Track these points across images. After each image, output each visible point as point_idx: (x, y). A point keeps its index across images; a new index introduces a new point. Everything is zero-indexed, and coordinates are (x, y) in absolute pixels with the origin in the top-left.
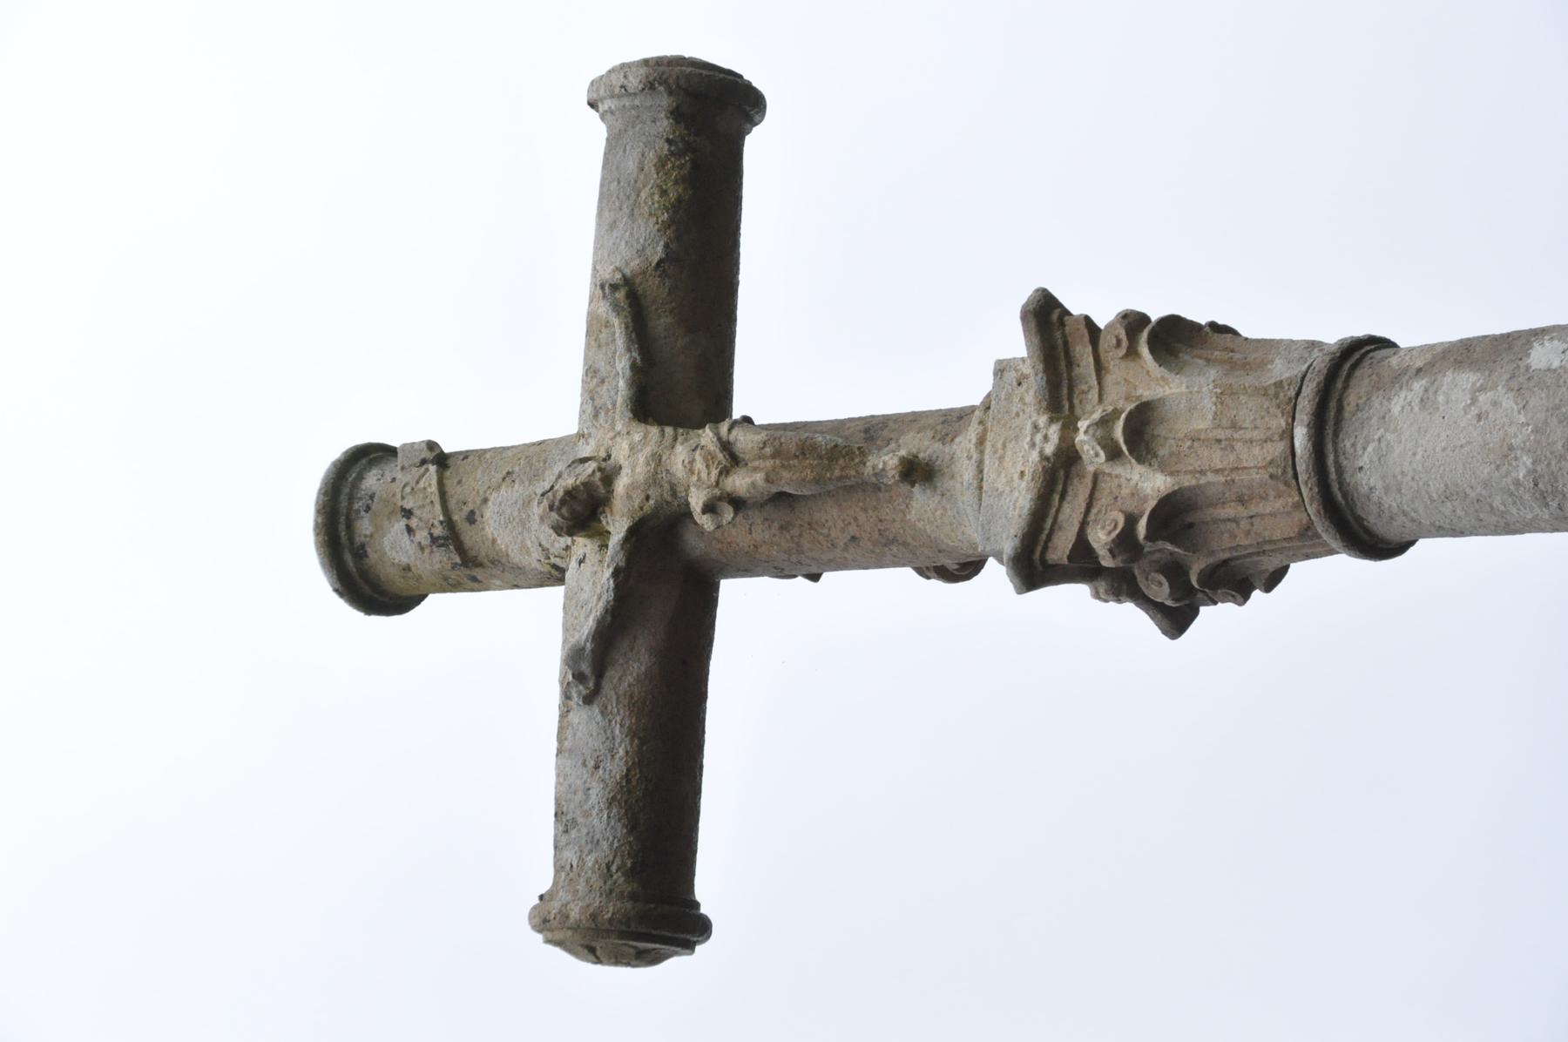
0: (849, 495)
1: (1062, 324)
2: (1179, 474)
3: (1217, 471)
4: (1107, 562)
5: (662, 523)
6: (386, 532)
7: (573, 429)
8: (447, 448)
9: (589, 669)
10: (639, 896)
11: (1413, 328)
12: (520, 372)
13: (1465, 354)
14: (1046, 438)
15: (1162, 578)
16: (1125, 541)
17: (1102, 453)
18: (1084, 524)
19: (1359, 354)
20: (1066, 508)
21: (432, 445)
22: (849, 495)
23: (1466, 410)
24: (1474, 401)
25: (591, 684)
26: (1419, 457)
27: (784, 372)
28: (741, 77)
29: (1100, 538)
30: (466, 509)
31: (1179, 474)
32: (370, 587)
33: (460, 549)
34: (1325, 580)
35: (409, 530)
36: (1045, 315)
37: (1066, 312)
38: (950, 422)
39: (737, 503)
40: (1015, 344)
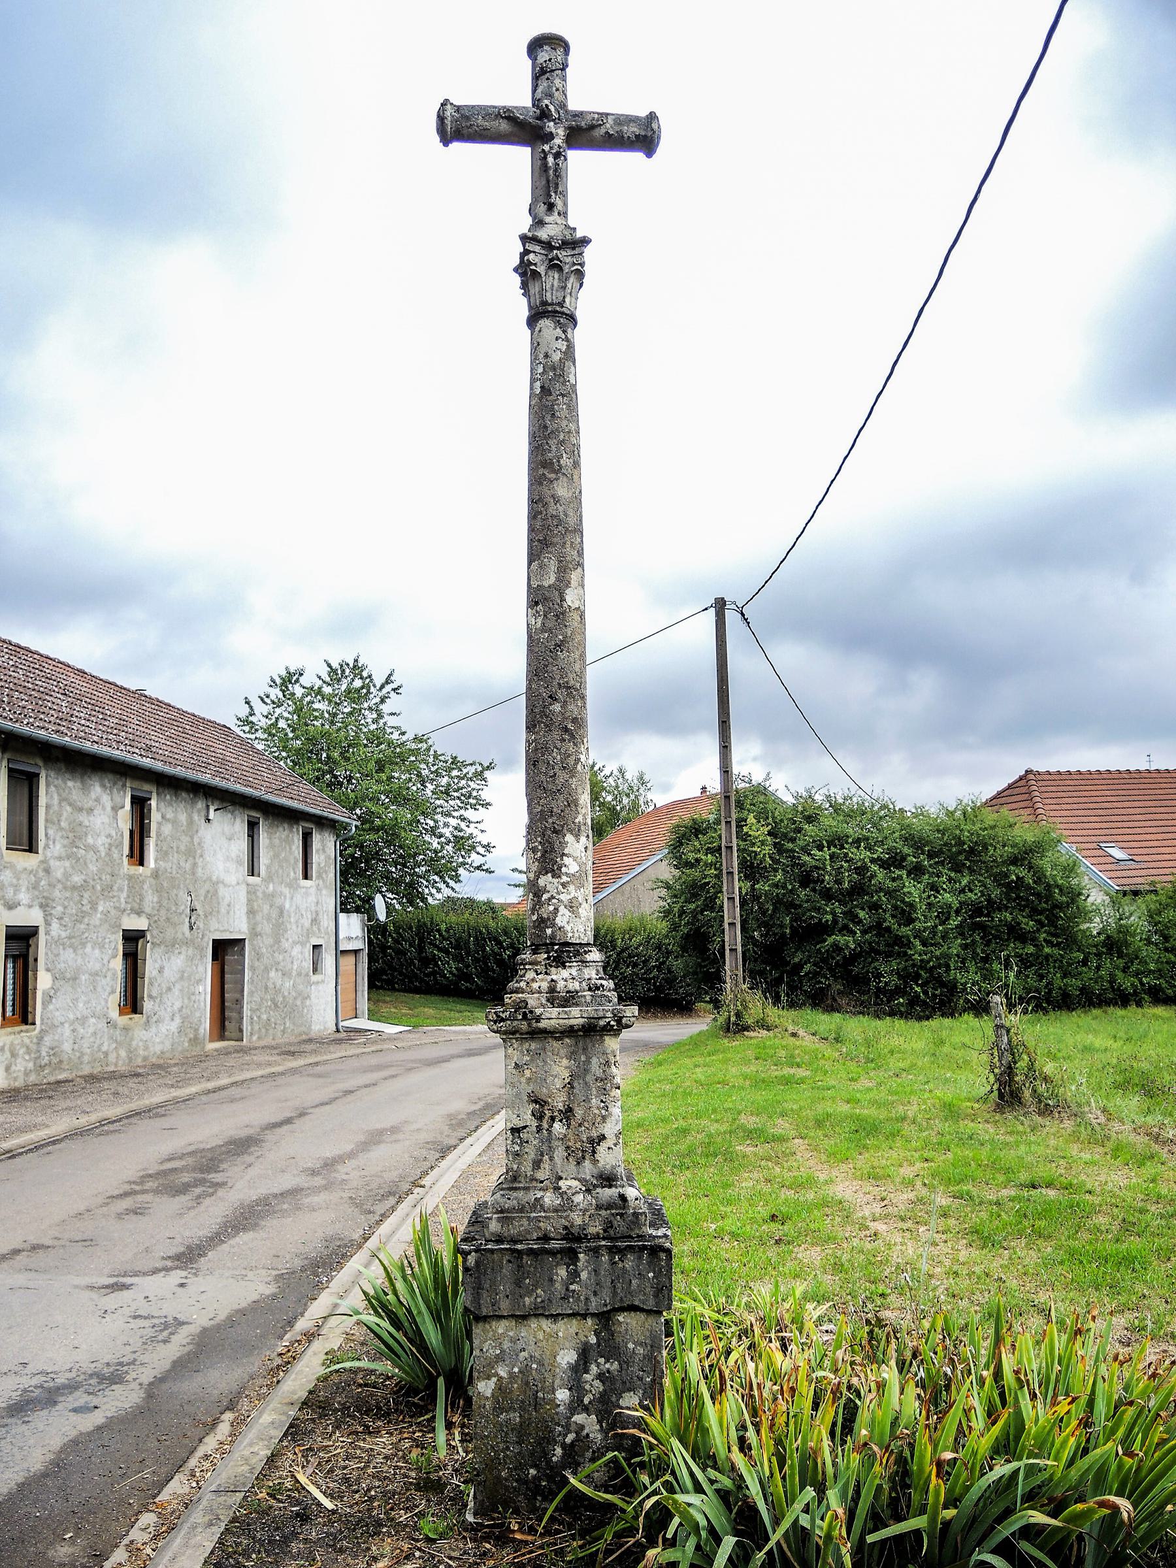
0: (548, 187)
2: (550, 266)
5: (544, 130)
6: (548, 53)
9: (508, 115)
11: (579, 335)
12: (583, 93)
13: (570, 347)
16: (530, 263)
19: (572, 319)
22: (548, 187)
27: (581, 165)
29: (531, 257)
31: (550, 266)
32: (536, 45)
34: (522, 309)
36: (585, 241)
38: (564, 214)
39: (545, 158)
40: (579, 234)
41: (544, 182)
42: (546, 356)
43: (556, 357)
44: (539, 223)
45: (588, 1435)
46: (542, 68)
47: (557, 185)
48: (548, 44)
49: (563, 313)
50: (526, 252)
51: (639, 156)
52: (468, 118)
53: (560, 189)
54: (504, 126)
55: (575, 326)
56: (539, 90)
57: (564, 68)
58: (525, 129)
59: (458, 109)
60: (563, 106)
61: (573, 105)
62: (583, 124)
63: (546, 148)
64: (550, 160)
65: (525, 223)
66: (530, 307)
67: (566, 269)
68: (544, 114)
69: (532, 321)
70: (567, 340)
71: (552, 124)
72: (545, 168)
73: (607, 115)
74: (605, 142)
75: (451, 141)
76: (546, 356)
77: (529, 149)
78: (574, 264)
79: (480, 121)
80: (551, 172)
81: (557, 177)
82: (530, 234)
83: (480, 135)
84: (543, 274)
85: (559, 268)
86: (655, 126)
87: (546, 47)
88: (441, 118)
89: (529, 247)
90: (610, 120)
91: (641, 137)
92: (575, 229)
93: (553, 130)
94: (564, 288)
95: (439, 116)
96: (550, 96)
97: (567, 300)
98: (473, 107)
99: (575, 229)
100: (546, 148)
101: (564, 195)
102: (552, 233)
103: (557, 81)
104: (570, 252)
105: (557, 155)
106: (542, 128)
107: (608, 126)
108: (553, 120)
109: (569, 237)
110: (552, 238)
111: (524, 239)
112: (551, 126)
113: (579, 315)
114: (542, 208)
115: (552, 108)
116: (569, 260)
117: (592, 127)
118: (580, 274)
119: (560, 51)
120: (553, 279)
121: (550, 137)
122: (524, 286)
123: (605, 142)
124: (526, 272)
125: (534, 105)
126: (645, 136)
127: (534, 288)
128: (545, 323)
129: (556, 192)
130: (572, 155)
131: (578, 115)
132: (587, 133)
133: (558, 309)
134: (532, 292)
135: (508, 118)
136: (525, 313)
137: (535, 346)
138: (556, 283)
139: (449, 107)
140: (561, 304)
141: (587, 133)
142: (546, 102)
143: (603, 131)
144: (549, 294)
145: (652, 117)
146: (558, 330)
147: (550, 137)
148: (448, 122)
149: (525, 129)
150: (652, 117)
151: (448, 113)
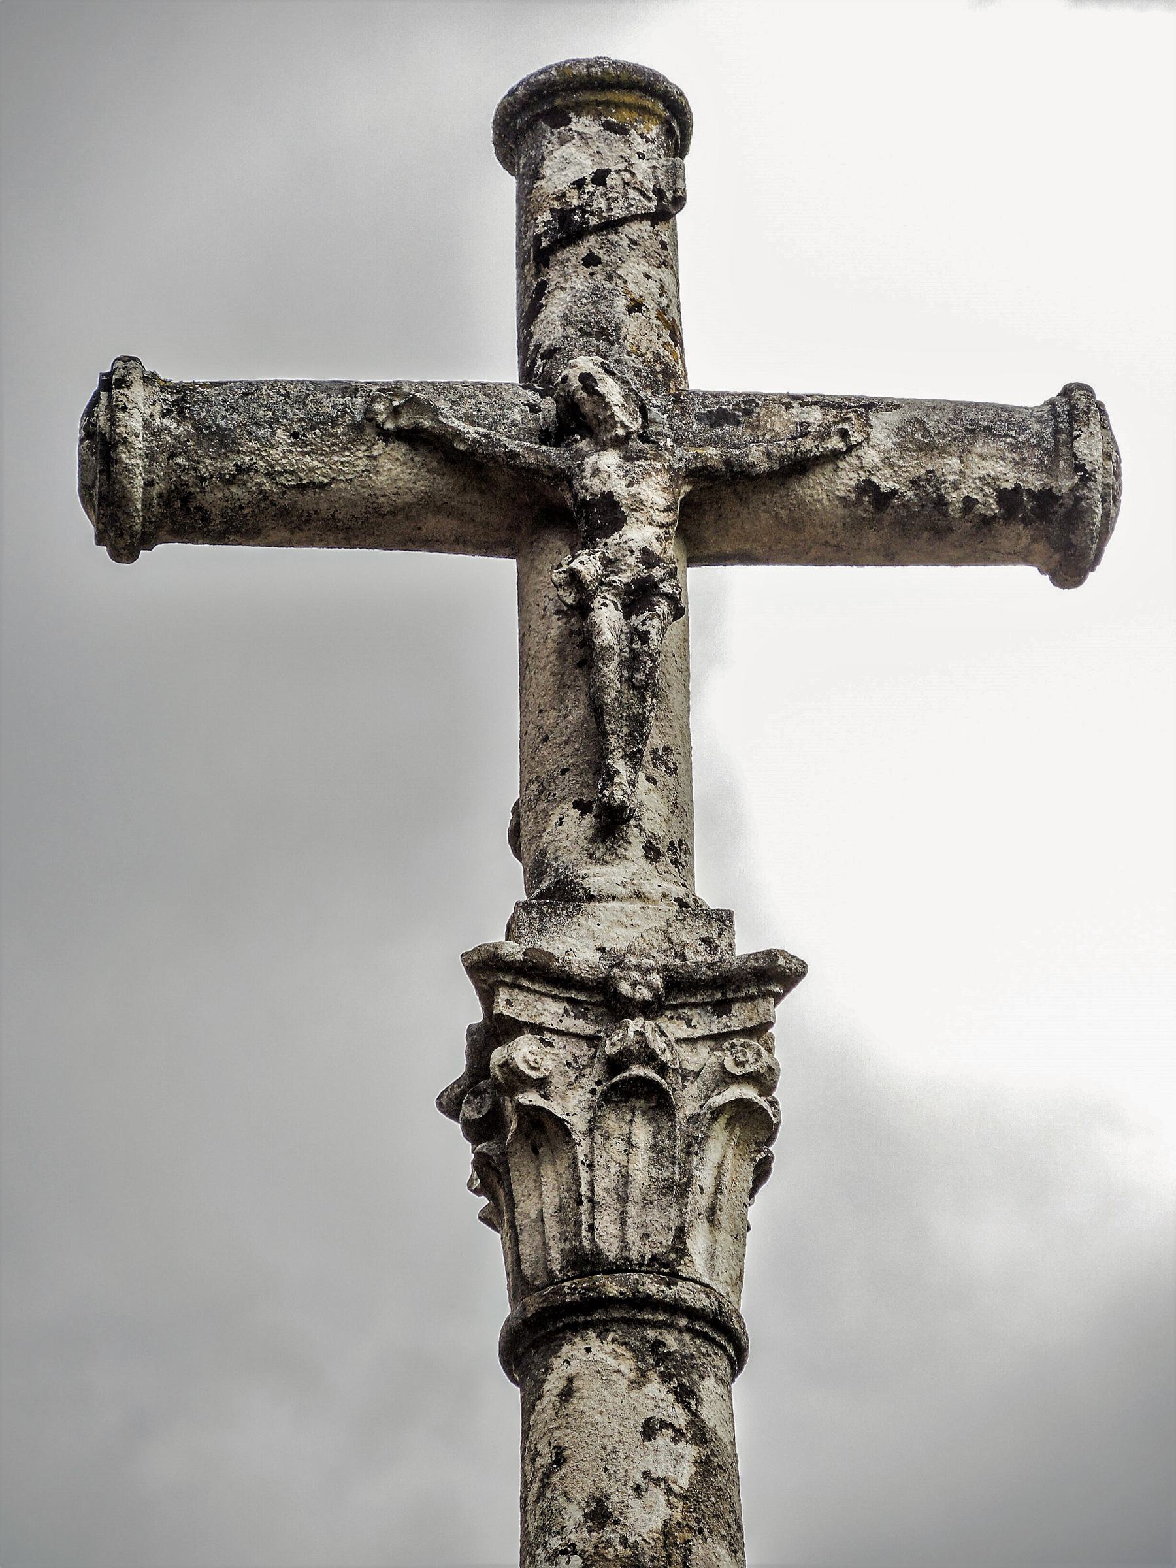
1: (765, 995)
3: (591, 1184)
4: (497, 1056)
5: (584, 488)
7: (708, 370)
8: (682, 218)
10: (175, 480)
12: (760, 311)
14: (635, 984)
15: (485, 1111)
16: (516, 1080)
17: (615, 1050)
18: (537, 1029)
19: (724, 1334)
20: (557, 1007)
21: (679, 202)
22: (603, 729)
23: (646, 1474)
24: (657, 1481)
25: (390, 425)
26: (598, 1418)
27: (761, 638)
28: (1093, 569)
29: (523, 1051)
30: (601, 253)
32: (532, 115)
33: (559, 244)
35: (579, 184)
36: (775, 975)
37: (778, 998)
38: (671, 852)
39: (582, 609)
40: (746, 943)
41: (578, 714)
42: (599, 1514)
43: (646, 1518)
44: (556, 895)
45: (667, 510)
46: (563, 216)
47: (638, 725)
48: (595, 109)
49: (676, 1308)
50: (496, 1030)
51: (1023, 582)
52: (223, 440)
53: (655, 740)
54: (393, 471)
55: (738, 1361)
56: (555, 307)
57: (666, 207)
58: (502, 489)
59: (181, 399)
60: (664, 375)
61: (713, 366)
62: (755, 455)
63: (588, 565)
64: (608, 619)
65: (489, 898)
66: (520, 1285)
67: (688, 1100)
68: (577, 419)
69: (527, 1347)
70: (699, 1433)
71: (610, 459)
72: (582, 652)
73: (867, 407)
74: (856, 526)
75: (148, 541)
76: (599, 1514)
77: (506, 568)
78: (726, 1078)
79: (282, 449)
80: (611, 671)
81: (641, 690)
82: (514, 951)
83: (284, 513)
84: (578, 1124)
85: (655, 1100)
86: (1088, 449)
87: (583, 124)
88: (101, 446)
89: (515, 1004)
90: (882, 433)
91: (1040, 501)
92: (724, 919)
93: (619, 488)
94: (679, 1189)
95: (90, 432)
96: (602, 334)
97: (698, 1243)
98: (250, 389)
99: (724, 919)
100: (588, 565)
101: (672, 765)
102: (619, 939)
103: (635, 272)
104: (705, 1023)
105: (638, 597)
106: (564, 478)
107: (871, 456)
108: (619, 443)
109: (697, 956)
110: (619, 961)
111: (487, 970)
112: (605, 470)
113: (753, 1310)
114: (569, 830)
115: (610, 389)
116: (698, 1058)
117: (799, 467)
118: (754, 1124)
119: (646, 138)
120: (627, 1150)
121: (607, 515)
122: (491, 1176)
123: (856, 526)
124: (500, 1121)
125: (527, 375)
126: (1046, 498)
127: (539, 1193)
128: (594, 1362)
129: (634, 759)
130: (698, 581)
131: (734, 412)
132: (764, 490)
133: (652, 1287)
134: (527, 1208)
135: (412, 437)
136: (496, 1308)
137: (544, 1470)
138: (641, 1168)
139: (137, 392)
140: (667, 1266)
141: (764, 490)
142: (586, 363)
143: (846, 478)
144: (606, 1223)
145: (1075, 409)
146: (655, 1388)
147: (607, 515)
148: (133, 457)
149: (502, 489)
150: (1075, 409)
151: (133, 422)
